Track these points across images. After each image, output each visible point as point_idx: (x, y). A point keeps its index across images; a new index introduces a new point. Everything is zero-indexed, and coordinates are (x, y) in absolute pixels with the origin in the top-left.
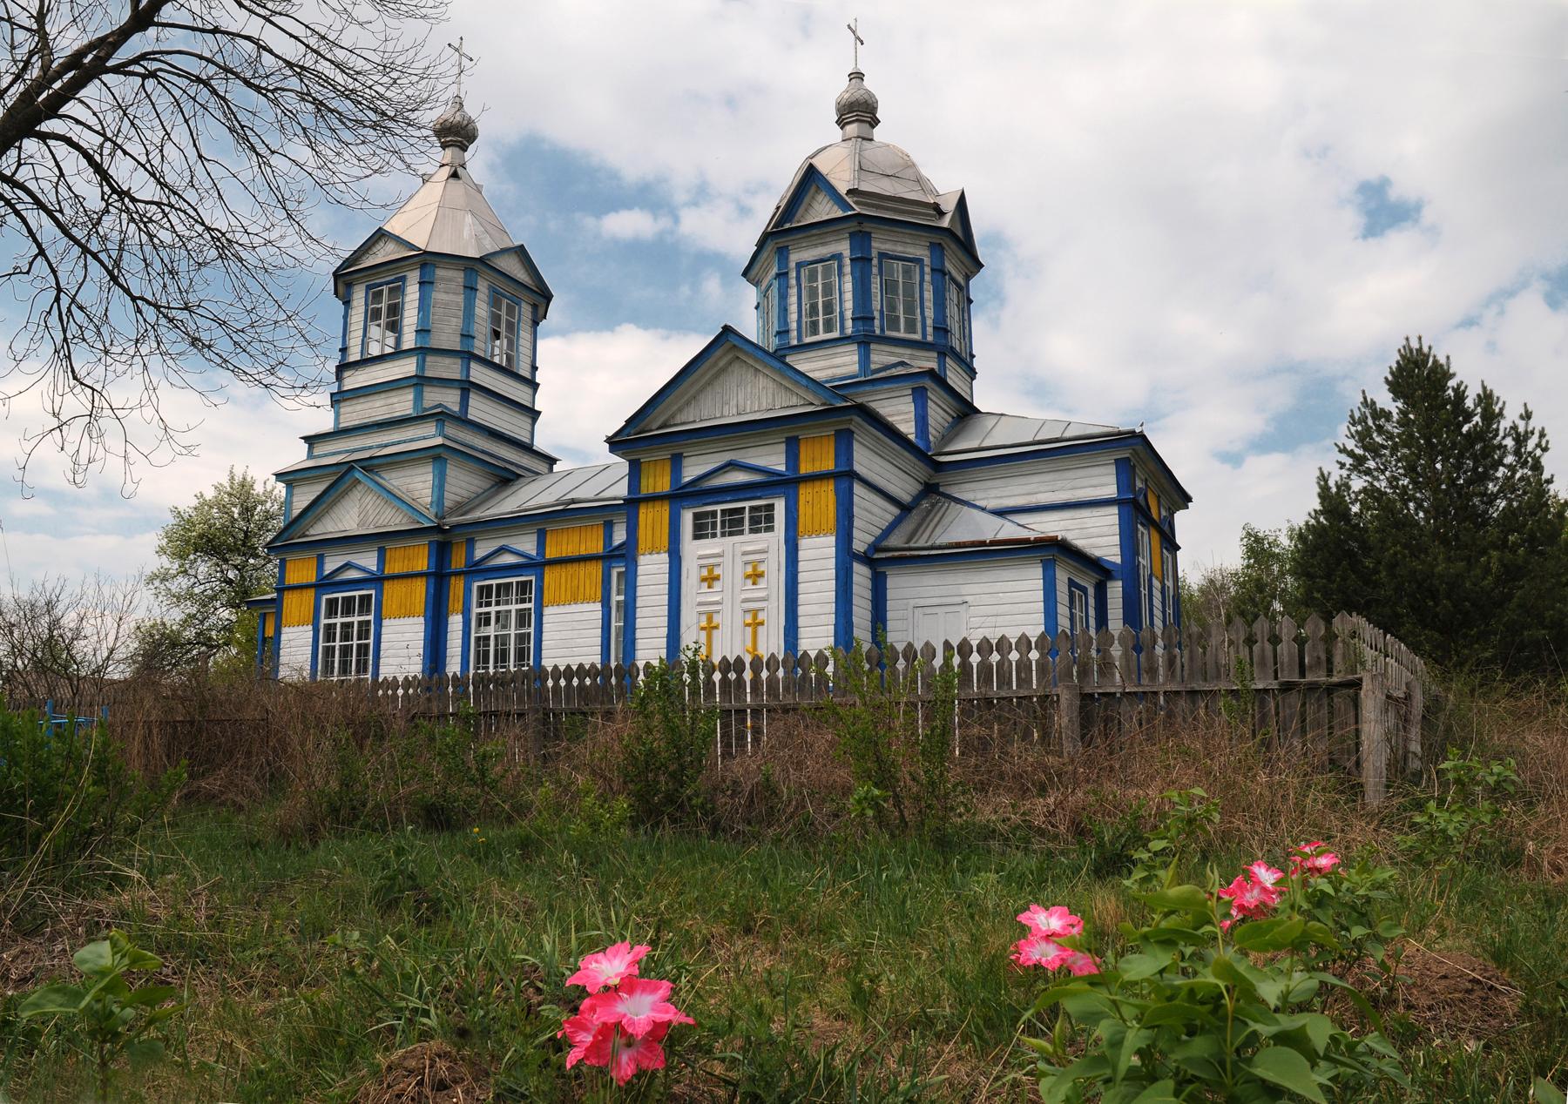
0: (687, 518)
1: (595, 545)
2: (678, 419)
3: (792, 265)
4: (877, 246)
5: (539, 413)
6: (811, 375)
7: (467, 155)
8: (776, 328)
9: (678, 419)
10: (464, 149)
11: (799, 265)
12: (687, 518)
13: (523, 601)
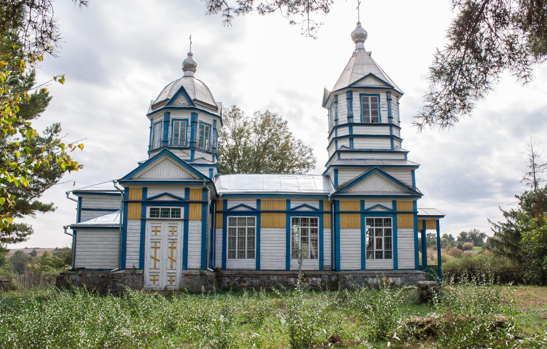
0: (148, 209)
1: (283, 207)
2: (143, 177)
3: (171, 120)
4: (173, 116)
5: (402, 140)
6: (181, 158)
7: (365, 44)
8: (334, 119)
9: (143, 177)
10: (363, 42)
11: (173, 120)
12: (148, 209)
13: (305, 225)
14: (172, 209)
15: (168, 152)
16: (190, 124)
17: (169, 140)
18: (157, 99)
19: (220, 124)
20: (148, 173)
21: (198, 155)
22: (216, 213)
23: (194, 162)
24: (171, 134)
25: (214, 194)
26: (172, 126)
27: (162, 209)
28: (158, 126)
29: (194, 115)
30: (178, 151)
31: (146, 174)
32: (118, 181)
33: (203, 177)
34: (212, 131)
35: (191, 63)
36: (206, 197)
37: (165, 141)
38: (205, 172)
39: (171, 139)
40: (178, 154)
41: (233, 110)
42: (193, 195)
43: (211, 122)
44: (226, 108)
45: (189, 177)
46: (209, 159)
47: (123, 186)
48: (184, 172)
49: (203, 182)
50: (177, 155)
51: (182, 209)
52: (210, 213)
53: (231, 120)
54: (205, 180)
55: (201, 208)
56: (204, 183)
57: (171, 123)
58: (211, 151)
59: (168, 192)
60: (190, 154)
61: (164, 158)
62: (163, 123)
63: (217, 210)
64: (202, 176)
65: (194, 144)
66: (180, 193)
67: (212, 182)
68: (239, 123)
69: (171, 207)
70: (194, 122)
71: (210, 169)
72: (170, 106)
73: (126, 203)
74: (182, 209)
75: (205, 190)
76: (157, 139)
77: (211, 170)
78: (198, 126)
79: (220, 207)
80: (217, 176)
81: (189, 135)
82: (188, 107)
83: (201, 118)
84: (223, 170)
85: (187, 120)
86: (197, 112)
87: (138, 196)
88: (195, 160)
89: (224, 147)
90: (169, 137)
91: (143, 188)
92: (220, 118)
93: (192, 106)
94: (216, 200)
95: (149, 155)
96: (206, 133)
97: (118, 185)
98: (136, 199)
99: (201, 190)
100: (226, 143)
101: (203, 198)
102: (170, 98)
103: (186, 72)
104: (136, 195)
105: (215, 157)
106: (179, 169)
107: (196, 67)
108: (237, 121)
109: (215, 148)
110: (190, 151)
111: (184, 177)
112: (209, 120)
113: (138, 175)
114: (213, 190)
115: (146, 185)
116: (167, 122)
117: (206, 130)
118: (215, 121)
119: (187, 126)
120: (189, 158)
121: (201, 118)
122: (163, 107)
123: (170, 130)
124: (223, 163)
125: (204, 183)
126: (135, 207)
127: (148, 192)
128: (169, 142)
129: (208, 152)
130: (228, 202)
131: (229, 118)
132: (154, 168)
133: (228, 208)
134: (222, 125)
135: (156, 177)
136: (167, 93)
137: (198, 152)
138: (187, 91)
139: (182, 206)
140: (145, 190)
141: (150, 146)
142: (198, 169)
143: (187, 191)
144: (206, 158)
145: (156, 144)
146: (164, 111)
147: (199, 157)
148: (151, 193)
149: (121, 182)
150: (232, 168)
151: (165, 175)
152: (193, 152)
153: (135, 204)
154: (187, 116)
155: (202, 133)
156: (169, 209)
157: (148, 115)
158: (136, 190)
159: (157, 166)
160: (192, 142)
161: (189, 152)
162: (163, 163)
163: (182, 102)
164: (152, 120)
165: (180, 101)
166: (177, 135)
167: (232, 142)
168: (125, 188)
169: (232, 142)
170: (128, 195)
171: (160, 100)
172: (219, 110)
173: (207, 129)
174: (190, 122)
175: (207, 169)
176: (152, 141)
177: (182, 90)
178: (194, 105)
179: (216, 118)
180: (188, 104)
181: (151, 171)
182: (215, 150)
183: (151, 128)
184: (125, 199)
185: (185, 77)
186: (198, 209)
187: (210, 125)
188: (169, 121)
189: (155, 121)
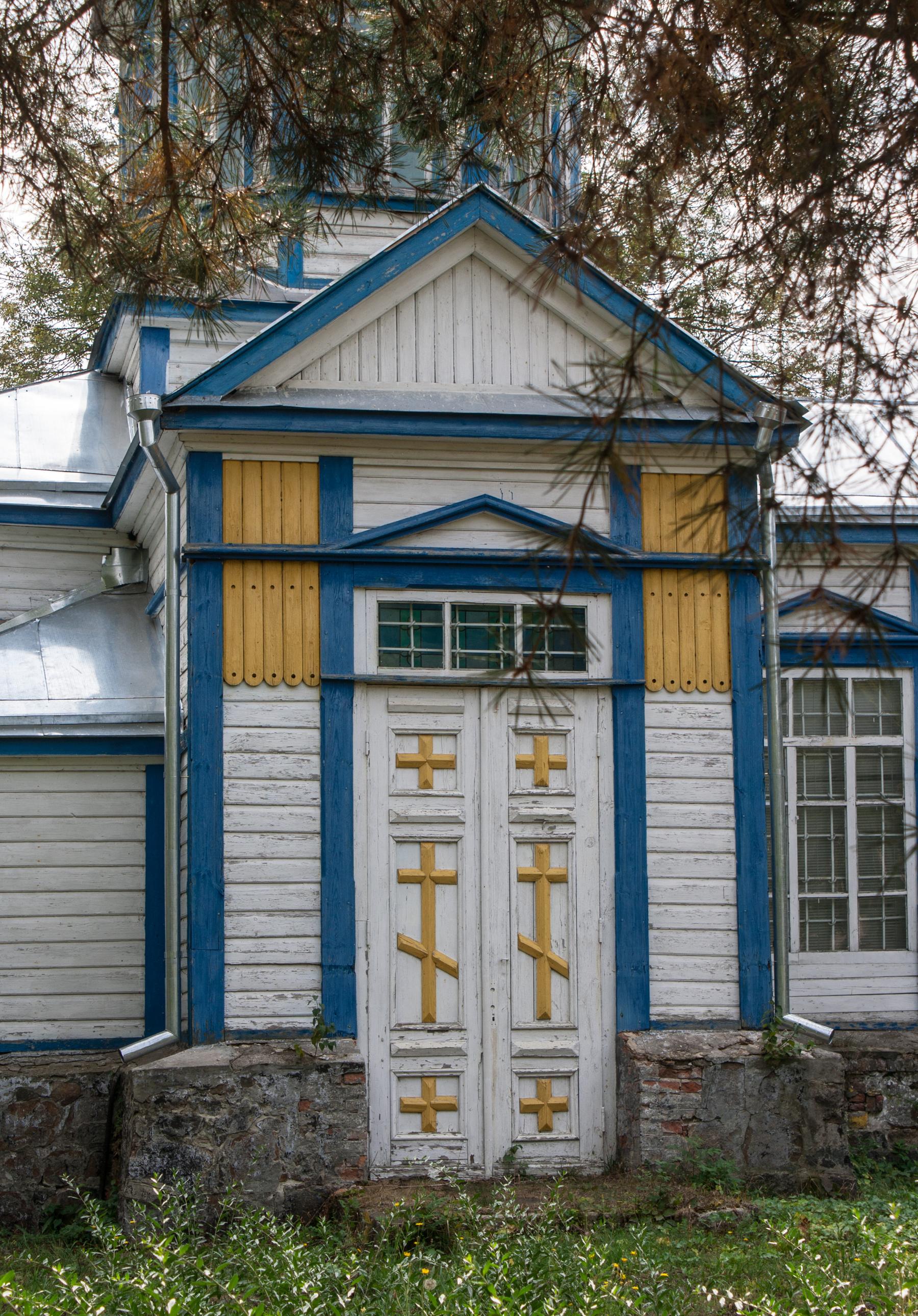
0: (365, 608)
12: (365, 608)
20: (349, 357)
31: (331, 364)
55: (720, 604)
61: (462, 251)
87: (292, 516)
98: (273, 539)
127: (362, 488)
140: (335, 477)
148: (383, 500)
151: (464, 374)
153: (273, 574)
158: (272, 475)
159: (408, 313)
162: (445, 287)
170: (220, 508)
181: (369, 342)
186: (703, 602)
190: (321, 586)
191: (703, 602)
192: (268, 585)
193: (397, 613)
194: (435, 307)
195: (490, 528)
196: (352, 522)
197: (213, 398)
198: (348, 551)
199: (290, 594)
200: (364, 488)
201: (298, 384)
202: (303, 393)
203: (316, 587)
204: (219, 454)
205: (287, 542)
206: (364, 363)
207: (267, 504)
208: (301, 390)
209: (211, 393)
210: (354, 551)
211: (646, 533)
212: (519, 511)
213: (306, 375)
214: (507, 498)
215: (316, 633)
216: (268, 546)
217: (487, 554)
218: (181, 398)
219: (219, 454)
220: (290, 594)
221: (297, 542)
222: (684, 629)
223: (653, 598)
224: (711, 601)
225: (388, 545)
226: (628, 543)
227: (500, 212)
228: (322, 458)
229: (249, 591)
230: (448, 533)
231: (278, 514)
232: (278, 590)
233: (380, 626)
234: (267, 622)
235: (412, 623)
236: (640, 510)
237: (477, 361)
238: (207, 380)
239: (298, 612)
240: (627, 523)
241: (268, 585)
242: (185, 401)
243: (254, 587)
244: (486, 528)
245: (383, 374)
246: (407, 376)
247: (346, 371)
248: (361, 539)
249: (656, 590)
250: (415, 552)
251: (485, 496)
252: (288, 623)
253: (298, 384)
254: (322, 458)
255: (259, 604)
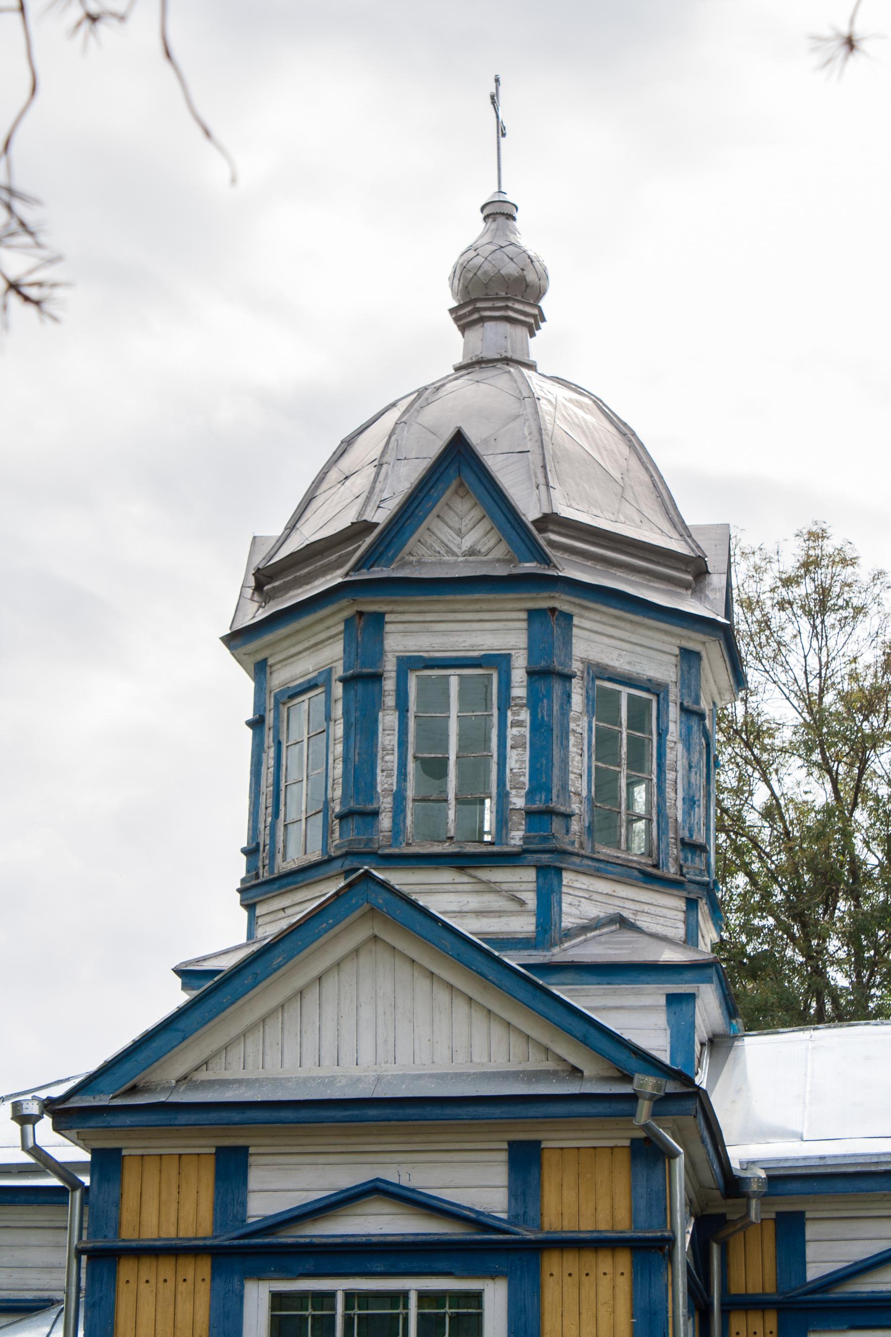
0: (257, 1298)
3: (390, 666)
4: (401, 639)
6: (466, 926)
11: (407, 664)
12: (257, 1298)
14: (424, 1297)
15: (381, 898)
16: (519, 691)
17: (386, 803)
18: (292, 527)
19: (724, 677)
20: (252, 1046)
21: (583, 898)
22: (725, 1312)
23: (557, 954)
24: (393, 759)
25: (710, 1176)
26: (402, 707)
27: (349, 1296)
28: (302, 717)
29: (550, 628)
30: (447, 876)
31: (236, 1053)
32: (50, 1106)
33: (633, 1063)
34: (674, 730)
35: (510, 269)
36: (661, 1202)
37: (359, 814)
38: (641, 1021)
39: (399, 797)
40: (448, 898)
41: (809, 565)
42: (569, 1196)
43: (662, 669)
44: (760, 554)
45: (536, 1062)
46: (662, 913)
47: (81, 1141)
48: (498, 1031)
49: (633, 1098)
50: (437, 904)
51: (495, 1297)
52: (690, 1312)
53: (794, 628)
54: (647, 1083)
55: (624, 1284)
56: (644, 1108)
57: (389, 685)
58: (672, 871)
59: (394, 1172)
60: (531, 899)
61: (361, 934)
62: (338, 689)
63: (737, 1287)
64: (627, 1057)
65: (557, 824)
66: (480, 1184)
67: (700, 1097)
68: (851, 649)
69: (413, 1285)
70: (547, 675)
71: (672, 999)
72: (378, 572)
73: (104, 1259)
74: (495, 1297)
75: (649, 1153)
76: (298, 801)
77: (679, 1003)
78: (577, 700)
79: (753, 1269)
80: (720, 1044)
81: (518, 761)
82: (501, 571)
83: (596, 641)
84: (769, 997)
85: (499, 662)
86: (563, 602)
87: (188, 1208)
88: (568, 934)
89: (752, 818)
90: (385, 782)
91: (221, 1152)
92: (725, 634)
93: (530, 567)
94: (720, 1221)
95: (250, 907)
96: (637, 750)
97: (45, 1133)
98: (169, 1232)
99: (623, 1160)
100: (761, 796)
101: (634, 1212)
102: (381, 517)
103: (475, 333)
104: (169, 1202)
105: (703, 908)
106: (461, 1008)
107: (540, 293)
108: (835, 639)
109: (701, 849)
110: (530, 875)
111: (500, 1063)
112: (647, 655)
113: (182, 1062)
114: (703, 1152)
115: (237, 1132)
116: (363, 681)
117: (633, 719)
118: (689, 658)
119: (505, 702)
120: (524, 925)
121: (596, 641)
122: (335, 579)
123: (387, 739)
124: (753, 932)
125: (644, 1108)
126: (166, 1291)
127: (257, 1178)
128: (386, 822)
129: (650, 878)
130: (811, 1231)
131: (778, 618)
132: (293, 1010)
133: (813, 1273)
134: (740, 680)
135: (310, 1069)
136: (360, 483)
137: (584, 882)
138: (494, 463)
139: (493, 1275)
140: (231, 1167)
141: (251, 852)
142: (586, 998)
143: (525, 1161)
144: (643, 922)
145: (296, 834)
146: (345, 609)
147: (593, 911)
148: (276, 1188)
149: (64, 1113)
150: (816, 960)
151: (367, 1056)
152: (549, 877)
153: (166, 1268)
154: (503, 632)
155: (605, 743)
156: (399, 1298)
157: (235, 639)
158: (171, 1168)
159: (311, 997)
160: (540, 816)
161: (523, 880)
162: (348, 969)
163: (458, 539)
164: (260, 671)
165: (445, 534)
166: (435, 768)
167: (803, 786)
168: (94, 1152)
169: (803, 786)
170: (118, 1204)
171: (312, 531)
172: (717, 580)
173: (638, 720)
174: (519, 676)
175: (654, 995)
176: (265, 818)
177: (459, 462)
178: (546, 560)
179: (695, 641)
180: (501, 551)
181: (273, 1030)
182: (698, 862)
183: (257, 724)
184: (93, 1235)
185: (473, 365)
186: (605, 1282)
187: (657, 689)
188: (378, 677)
189: (281, 677)
190: (213, 1279)
191: (605, 1282)
192: (161, 1279)
193: (389, 1301)
194: (339, 990)
195: (386, 1211)
196: (245, 1211)
197: (103, 1097)
198: (236, 1242)
199: (182, 1287)
200: (258, 1177)
201: (203, 1075)
202: (224, 1083)
203: (208, 1278)
204: (119, 1150)
205: (181, 1235)
206: (267, 1051)
207: (164, 1196)
208: (202, 1082)
209: (101, 1092)
210: (242, 1241)
211: (545, 1212)
212: (409, 1194)
213: (210, 1066)
214: (404, 1182)
215: (205, 1326)
216: (144, 1240)
217: (374, 1239)
218: (72, 1100)
219: (119, 1150)
220: (182, 1287)
221: (191, 1235)
222: (583, 1311)
223: (551, 1279)
224: (614, 1280)
225: (282, 1234)
226: (525, 1222)
227: (387, 895)
228: (218, 1148)
229: (143, 1285)
230: (346, 1218)
231: (174, 1206)
232: (171, 1283)
233: (272, 1316)
234: (158, 1317)
235: (310, 1311)
236: (540, 1186)
237: (380, 1041)
238: (98, 1080)
239: (189, 1306)
240: (525, 1201)
241: (180, 1279)
242: (77, 1102)
243: (147, 1282)
244: (383, 1212)
245: (286, 1061)
246: (309, 1060)
247: (250, 1060)
248: (255, 1227)
249: (555, 1270)
250: (302, 1240)
251: (378, 1179)
252: (179, 1317)
253: (203, 1075)
254: (218, 1148)
255: (152, 1299)
